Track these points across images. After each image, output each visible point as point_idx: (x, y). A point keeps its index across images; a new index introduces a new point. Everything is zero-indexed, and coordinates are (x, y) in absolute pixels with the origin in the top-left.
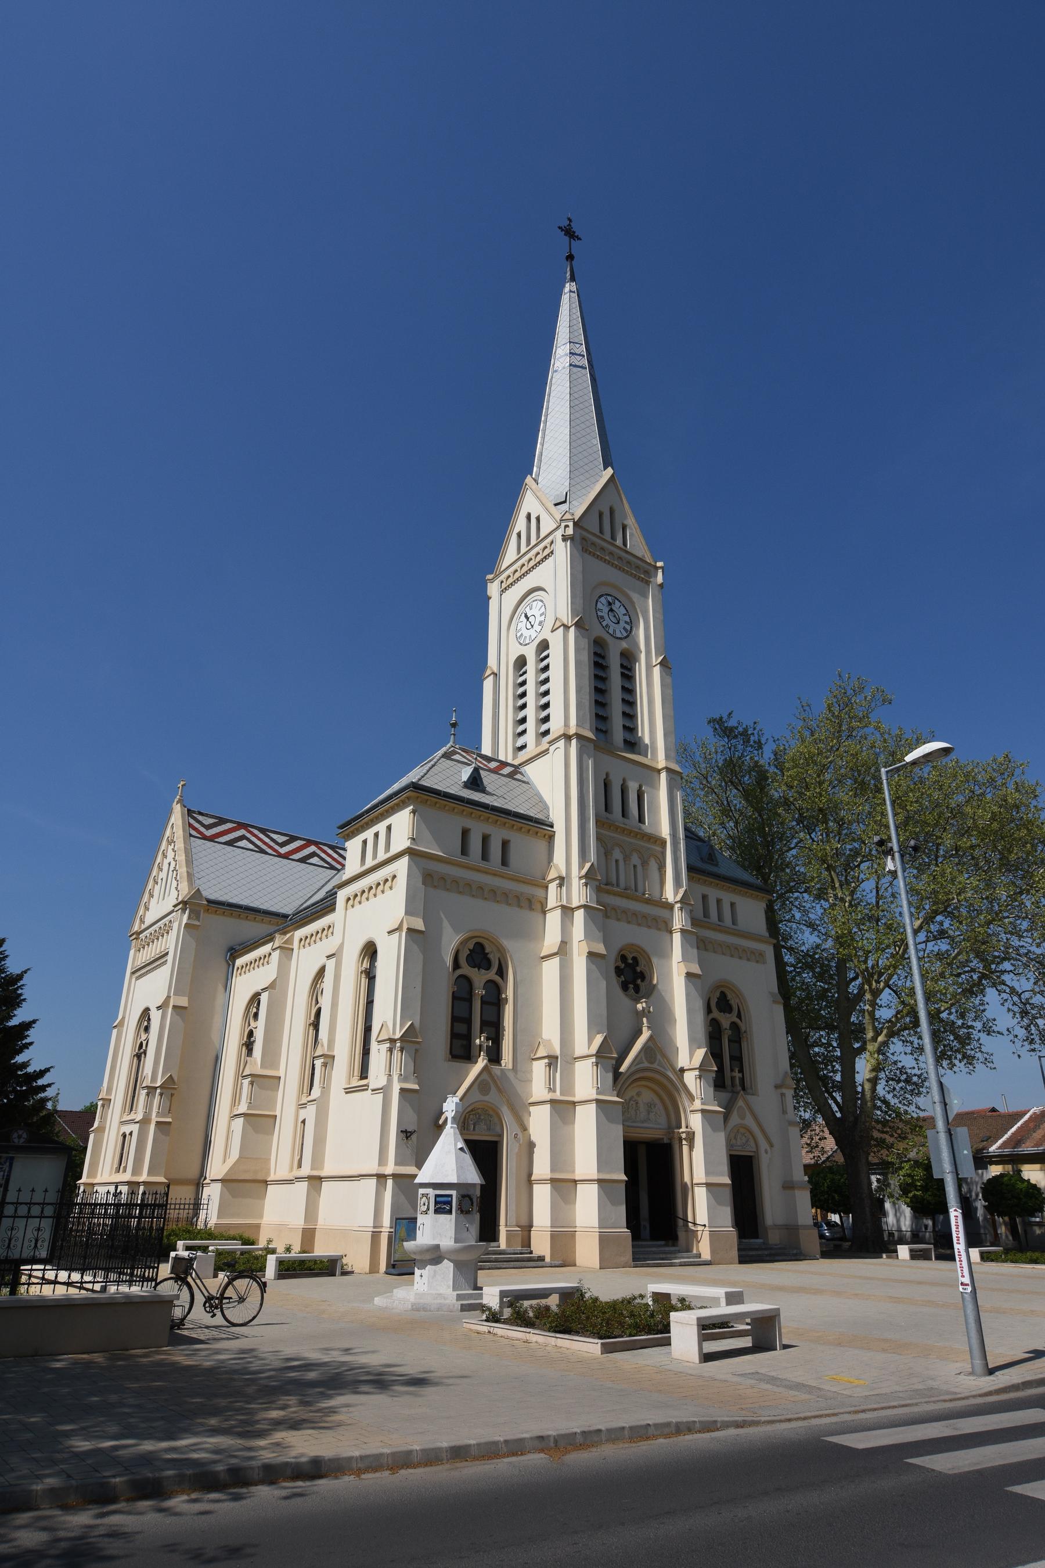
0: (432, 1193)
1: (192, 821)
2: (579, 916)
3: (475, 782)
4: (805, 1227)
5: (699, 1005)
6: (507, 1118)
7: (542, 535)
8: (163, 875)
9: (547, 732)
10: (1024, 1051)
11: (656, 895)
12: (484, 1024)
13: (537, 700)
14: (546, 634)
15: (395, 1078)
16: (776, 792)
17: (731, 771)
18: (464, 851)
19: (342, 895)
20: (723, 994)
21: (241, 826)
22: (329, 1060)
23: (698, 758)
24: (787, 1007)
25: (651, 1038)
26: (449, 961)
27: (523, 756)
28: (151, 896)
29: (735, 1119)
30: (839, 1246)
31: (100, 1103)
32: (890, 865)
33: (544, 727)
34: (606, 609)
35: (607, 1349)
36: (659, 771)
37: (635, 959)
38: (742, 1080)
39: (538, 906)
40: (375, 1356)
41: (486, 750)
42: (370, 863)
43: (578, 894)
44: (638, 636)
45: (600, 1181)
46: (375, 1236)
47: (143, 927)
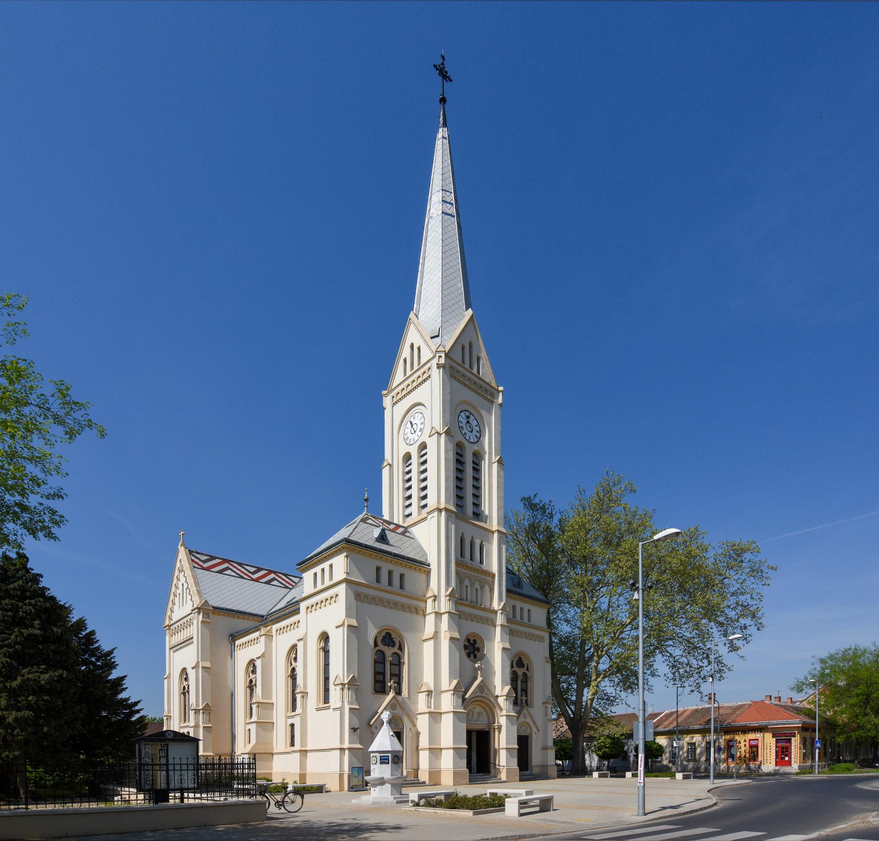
0: (378, 755)
1: (193, 558)
2: (445, 618)
3: (382, 538)
4: (551, 766)
5: (508, 664)
6: (406, 720)
7: (422, 363)
8: (180, 591)
9: (425, 506)
10: (670, 685)
11: (488, 606)
12: (392, 675)
13: (419, 485)
14: (425, 438)
15: (346, 703)
16: (558, 544)
17: (532, 530)
18: (378, 580)
19: (303, 606)
20: (520, 658)
21: (225, 561)
22: (305, 694)
23: (512, 523)
24: (553, 665)
25: (482, 681)
26: (372, 642)
27: (409, 521)
28: (174, 604)
29: (522, 719)
30: (562, 774)
31: (165, 718)
32: (636, 596)
33: (423, 503)
34: (465, 421)
35: (475, 814)
36: (493, 532)
37: (474, 641)
38: (526, 701)
39: (421, 612)
40: (371, 820)
41: (386, 517)
42: (320, 587)
43: (445, 605)
44: (484, 441)
45: (454, 748)
46: (341, 776)
47: (172, 622)
